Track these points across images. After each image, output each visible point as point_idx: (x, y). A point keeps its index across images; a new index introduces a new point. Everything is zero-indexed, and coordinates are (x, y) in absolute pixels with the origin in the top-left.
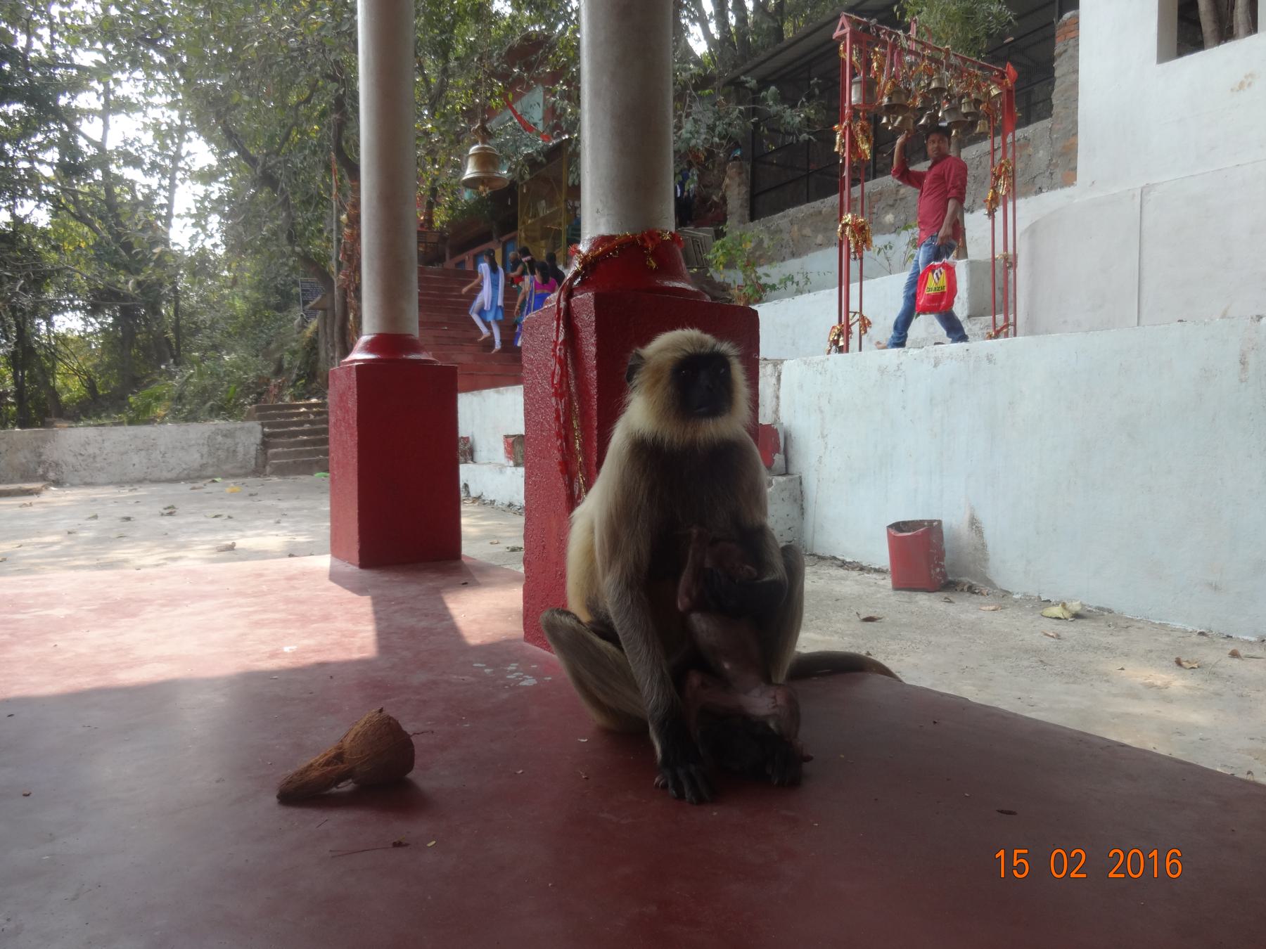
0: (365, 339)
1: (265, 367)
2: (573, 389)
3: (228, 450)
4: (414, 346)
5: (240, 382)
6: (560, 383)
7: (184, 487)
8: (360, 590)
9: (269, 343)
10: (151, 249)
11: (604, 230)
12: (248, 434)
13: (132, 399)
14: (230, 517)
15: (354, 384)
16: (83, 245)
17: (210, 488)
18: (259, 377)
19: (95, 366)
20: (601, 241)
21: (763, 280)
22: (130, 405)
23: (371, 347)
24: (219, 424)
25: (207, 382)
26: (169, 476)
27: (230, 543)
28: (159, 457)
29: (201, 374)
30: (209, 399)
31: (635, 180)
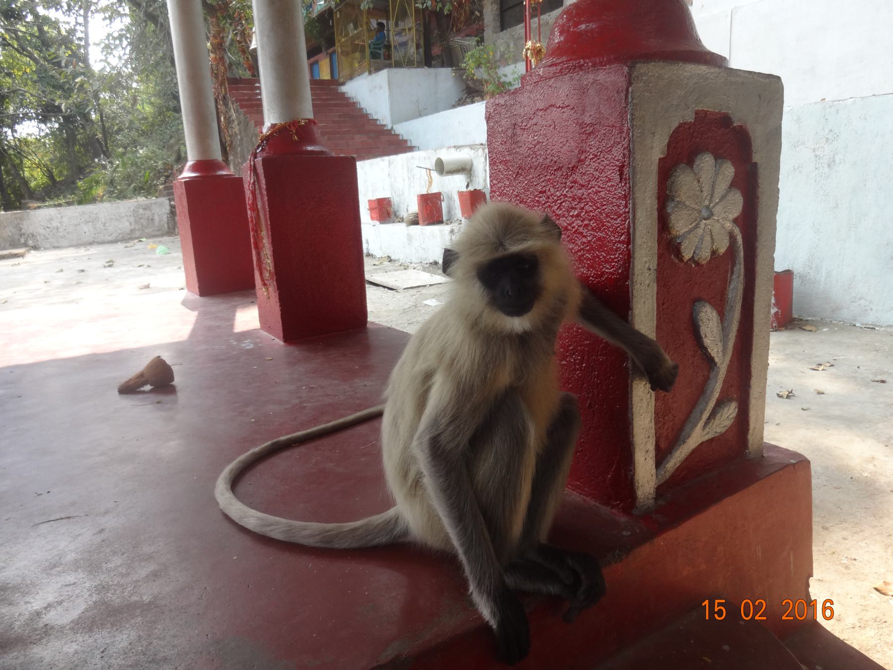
0: (190, 163)
1: (169, 157)
2: (259, 207)
3: (148, 219)
5: (153, 169)
6: (253, 204)
7: (120, 246)
8: (193, 309)
12: (159, 207)
13: (80, 183)
15: (184, 192)
17: (139, 246)
18: (164, 164)
20: (273, 126)
21: (503, 79)
22: (77, 188)
23: (195, 168)
24: (141, 200)
26: (110, 238)
27: (146, 284)
28: (102, 226)
29: (124, 164)
30: (132, 182)
31: (288, 93)
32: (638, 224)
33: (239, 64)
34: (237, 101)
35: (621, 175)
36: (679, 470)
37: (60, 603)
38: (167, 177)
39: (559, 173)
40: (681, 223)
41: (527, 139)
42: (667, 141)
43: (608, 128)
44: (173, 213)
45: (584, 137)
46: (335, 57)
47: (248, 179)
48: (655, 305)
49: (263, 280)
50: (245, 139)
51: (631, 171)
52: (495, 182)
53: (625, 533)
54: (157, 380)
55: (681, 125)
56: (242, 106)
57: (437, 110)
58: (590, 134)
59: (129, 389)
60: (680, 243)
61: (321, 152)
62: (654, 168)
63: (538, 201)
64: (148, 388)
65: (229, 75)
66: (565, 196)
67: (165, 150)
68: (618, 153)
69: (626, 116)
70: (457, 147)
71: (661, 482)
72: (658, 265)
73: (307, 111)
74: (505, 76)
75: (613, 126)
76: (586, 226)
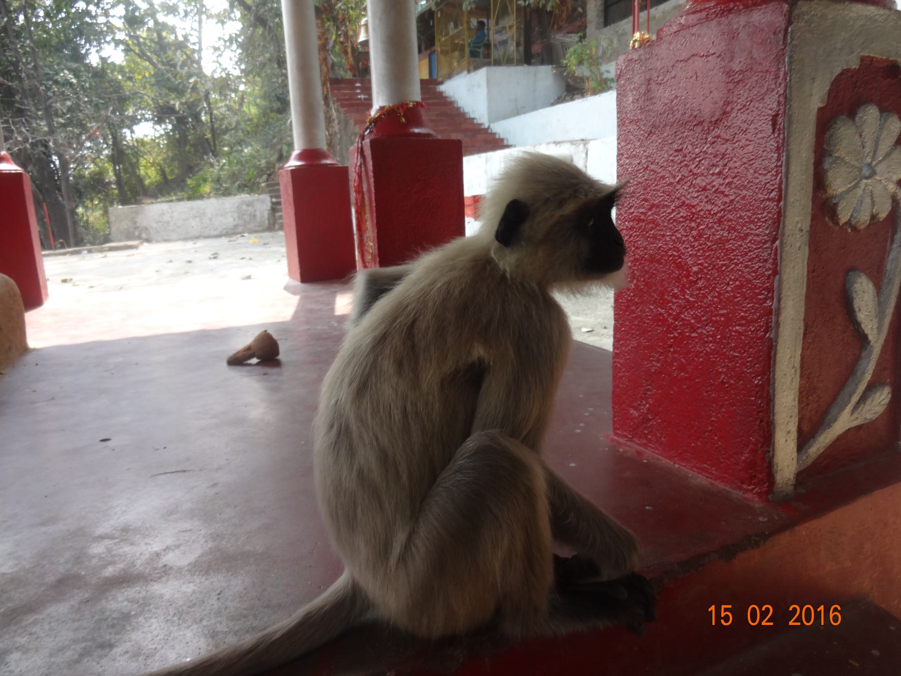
0: (296, 152)
1: (272, 156)
3: (250, 215)
4: (324, 155)
5: (257, 167)
7: (224, 241)
8: (294, 293)
9: (274, 137)
10: (188, 79)
11: (382, 104)
12: (262, 203)
13: (189, 181)
14: (250, 259)
15: (290, 180)
16: (147, 74)
17: (241, 240)
18: (267, 163)
19: (164, 160)
20: (382, 108)
21: (605, 76)
22: (187, 185)
23: (301, 157)
24: (245, 197)
25: (235, 168)
26: (216, 233)
30: (237, 180)
32: (791, 179)
33: (341, 66)
34: (338, 100)
35: (774, 124)
36: (822, 457)
37: (178, 546)
38: (269, 175)
39: (699, 129)
40: (838, 182)
41: (663, 94)
42: (828, 88)
43: (761, 74)
44: (275, 208)
45: (731, 86)
46: (434, 57)
47: (352, 162)
48: (806, 270)
49: (364, 261)
50: (344, 138)
51: (786, 119)
52: (623, 144)
53: (761, 519)
54: (265, 353)
55: (844, 72)
56: (343, 106)
57: (535, 108)
58: (738, 82)
59: (237, 361)
60: (836, 204)
61: (428, 135)
62: (812, 118)
63: (672, 161)
64: (254, 361)
65: (331, 75)
66: (705, 152)
67: (268, 149)
68: (772, 102)
69: (784, 60)
70: (557, 143)
71: (802, 468)
72: (811, 226)
73: (415, 95)
74: (608, 72)
75: (767, 71)
76: (729, 184)
